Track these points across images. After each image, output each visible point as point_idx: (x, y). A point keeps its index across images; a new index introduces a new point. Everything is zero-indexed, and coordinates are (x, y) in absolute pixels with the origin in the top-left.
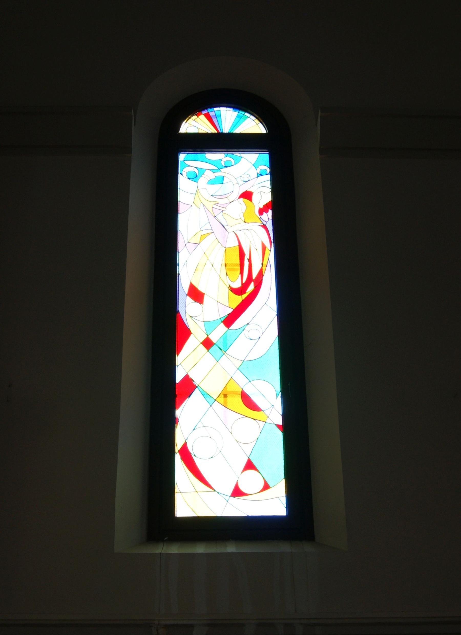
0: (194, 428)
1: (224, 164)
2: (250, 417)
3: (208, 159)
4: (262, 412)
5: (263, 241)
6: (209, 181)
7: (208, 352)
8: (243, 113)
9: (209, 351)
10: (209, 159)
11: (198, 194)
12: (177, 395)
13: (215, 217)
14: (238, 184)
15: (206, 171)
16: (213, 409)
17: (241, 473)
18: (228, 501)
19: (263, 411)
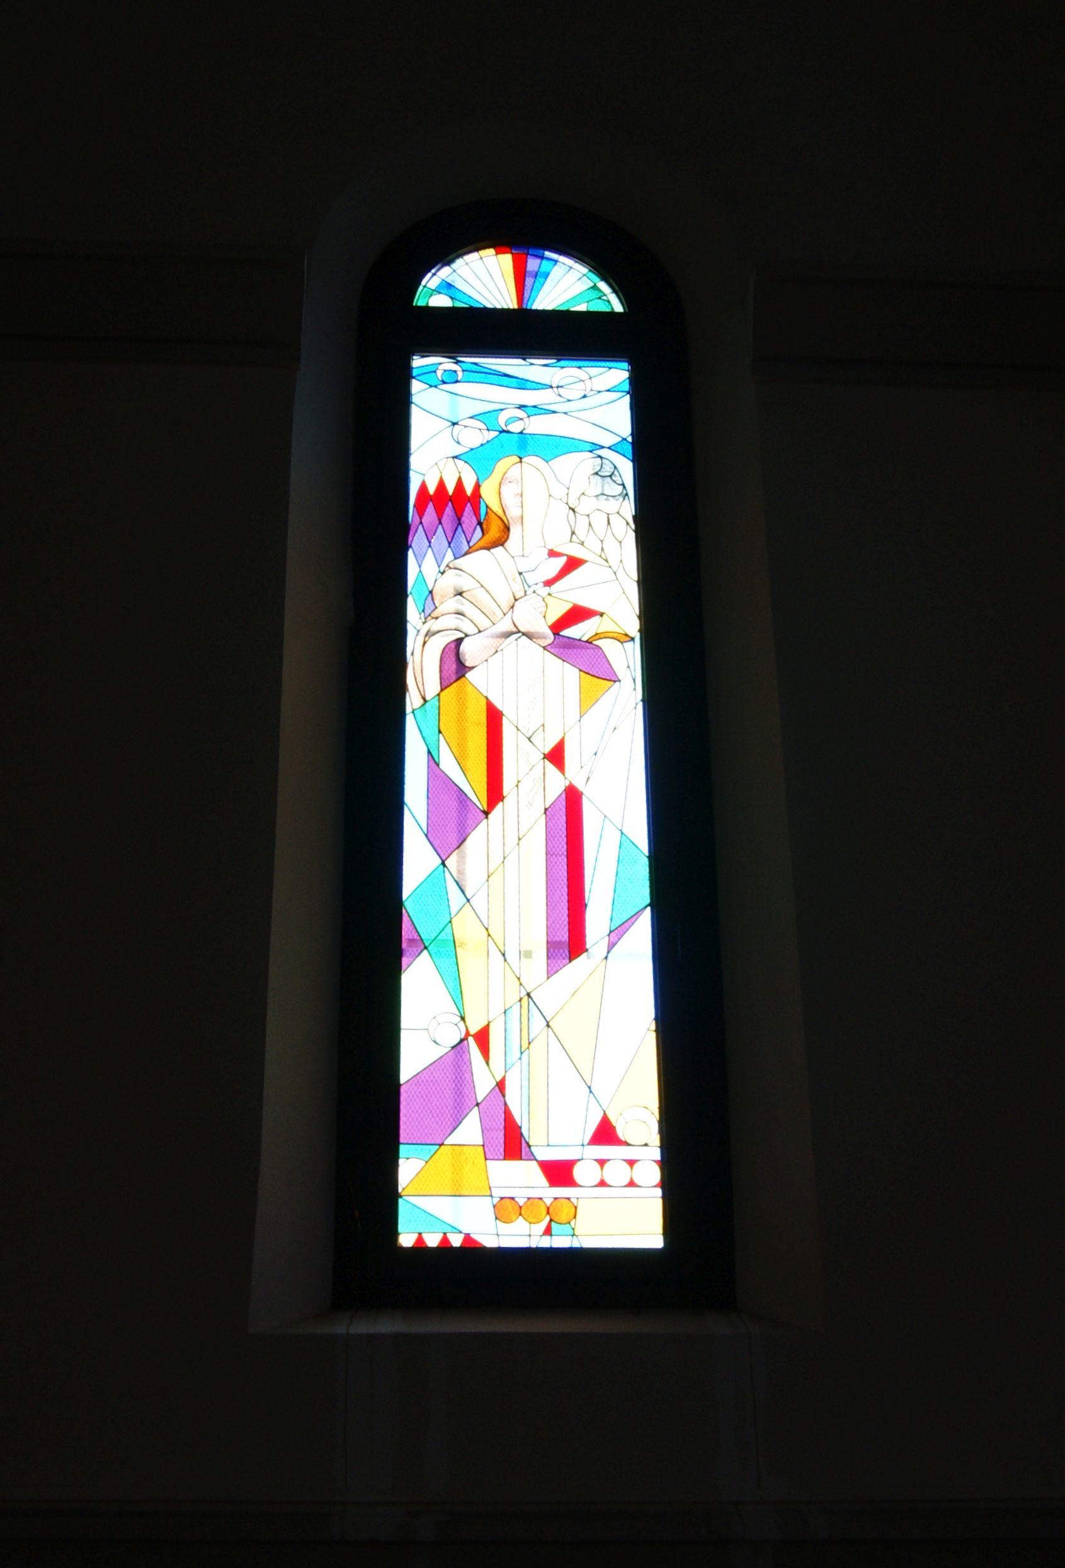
0: (500, 954)
1: (442, 377)
2: (467, 783)
3: (540, 457)
4: (491, 1024)
5: (445, 479)
6: (580, 640)
7: (553, 1237)
8: (421, 288)
9: (553, 1233)
10: (537, 456)
11: (499, 294)
12: (542, 258)
13: (621, 1114)
14: (579, 1199)
15: (437, 287)
16: (505, 1056)
17: (487, 1063)
18: (499, 1234)
19: (489, 1022)
